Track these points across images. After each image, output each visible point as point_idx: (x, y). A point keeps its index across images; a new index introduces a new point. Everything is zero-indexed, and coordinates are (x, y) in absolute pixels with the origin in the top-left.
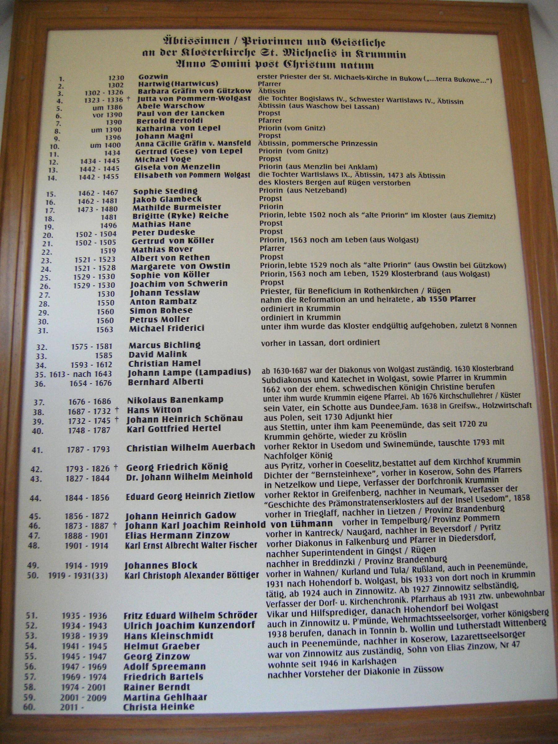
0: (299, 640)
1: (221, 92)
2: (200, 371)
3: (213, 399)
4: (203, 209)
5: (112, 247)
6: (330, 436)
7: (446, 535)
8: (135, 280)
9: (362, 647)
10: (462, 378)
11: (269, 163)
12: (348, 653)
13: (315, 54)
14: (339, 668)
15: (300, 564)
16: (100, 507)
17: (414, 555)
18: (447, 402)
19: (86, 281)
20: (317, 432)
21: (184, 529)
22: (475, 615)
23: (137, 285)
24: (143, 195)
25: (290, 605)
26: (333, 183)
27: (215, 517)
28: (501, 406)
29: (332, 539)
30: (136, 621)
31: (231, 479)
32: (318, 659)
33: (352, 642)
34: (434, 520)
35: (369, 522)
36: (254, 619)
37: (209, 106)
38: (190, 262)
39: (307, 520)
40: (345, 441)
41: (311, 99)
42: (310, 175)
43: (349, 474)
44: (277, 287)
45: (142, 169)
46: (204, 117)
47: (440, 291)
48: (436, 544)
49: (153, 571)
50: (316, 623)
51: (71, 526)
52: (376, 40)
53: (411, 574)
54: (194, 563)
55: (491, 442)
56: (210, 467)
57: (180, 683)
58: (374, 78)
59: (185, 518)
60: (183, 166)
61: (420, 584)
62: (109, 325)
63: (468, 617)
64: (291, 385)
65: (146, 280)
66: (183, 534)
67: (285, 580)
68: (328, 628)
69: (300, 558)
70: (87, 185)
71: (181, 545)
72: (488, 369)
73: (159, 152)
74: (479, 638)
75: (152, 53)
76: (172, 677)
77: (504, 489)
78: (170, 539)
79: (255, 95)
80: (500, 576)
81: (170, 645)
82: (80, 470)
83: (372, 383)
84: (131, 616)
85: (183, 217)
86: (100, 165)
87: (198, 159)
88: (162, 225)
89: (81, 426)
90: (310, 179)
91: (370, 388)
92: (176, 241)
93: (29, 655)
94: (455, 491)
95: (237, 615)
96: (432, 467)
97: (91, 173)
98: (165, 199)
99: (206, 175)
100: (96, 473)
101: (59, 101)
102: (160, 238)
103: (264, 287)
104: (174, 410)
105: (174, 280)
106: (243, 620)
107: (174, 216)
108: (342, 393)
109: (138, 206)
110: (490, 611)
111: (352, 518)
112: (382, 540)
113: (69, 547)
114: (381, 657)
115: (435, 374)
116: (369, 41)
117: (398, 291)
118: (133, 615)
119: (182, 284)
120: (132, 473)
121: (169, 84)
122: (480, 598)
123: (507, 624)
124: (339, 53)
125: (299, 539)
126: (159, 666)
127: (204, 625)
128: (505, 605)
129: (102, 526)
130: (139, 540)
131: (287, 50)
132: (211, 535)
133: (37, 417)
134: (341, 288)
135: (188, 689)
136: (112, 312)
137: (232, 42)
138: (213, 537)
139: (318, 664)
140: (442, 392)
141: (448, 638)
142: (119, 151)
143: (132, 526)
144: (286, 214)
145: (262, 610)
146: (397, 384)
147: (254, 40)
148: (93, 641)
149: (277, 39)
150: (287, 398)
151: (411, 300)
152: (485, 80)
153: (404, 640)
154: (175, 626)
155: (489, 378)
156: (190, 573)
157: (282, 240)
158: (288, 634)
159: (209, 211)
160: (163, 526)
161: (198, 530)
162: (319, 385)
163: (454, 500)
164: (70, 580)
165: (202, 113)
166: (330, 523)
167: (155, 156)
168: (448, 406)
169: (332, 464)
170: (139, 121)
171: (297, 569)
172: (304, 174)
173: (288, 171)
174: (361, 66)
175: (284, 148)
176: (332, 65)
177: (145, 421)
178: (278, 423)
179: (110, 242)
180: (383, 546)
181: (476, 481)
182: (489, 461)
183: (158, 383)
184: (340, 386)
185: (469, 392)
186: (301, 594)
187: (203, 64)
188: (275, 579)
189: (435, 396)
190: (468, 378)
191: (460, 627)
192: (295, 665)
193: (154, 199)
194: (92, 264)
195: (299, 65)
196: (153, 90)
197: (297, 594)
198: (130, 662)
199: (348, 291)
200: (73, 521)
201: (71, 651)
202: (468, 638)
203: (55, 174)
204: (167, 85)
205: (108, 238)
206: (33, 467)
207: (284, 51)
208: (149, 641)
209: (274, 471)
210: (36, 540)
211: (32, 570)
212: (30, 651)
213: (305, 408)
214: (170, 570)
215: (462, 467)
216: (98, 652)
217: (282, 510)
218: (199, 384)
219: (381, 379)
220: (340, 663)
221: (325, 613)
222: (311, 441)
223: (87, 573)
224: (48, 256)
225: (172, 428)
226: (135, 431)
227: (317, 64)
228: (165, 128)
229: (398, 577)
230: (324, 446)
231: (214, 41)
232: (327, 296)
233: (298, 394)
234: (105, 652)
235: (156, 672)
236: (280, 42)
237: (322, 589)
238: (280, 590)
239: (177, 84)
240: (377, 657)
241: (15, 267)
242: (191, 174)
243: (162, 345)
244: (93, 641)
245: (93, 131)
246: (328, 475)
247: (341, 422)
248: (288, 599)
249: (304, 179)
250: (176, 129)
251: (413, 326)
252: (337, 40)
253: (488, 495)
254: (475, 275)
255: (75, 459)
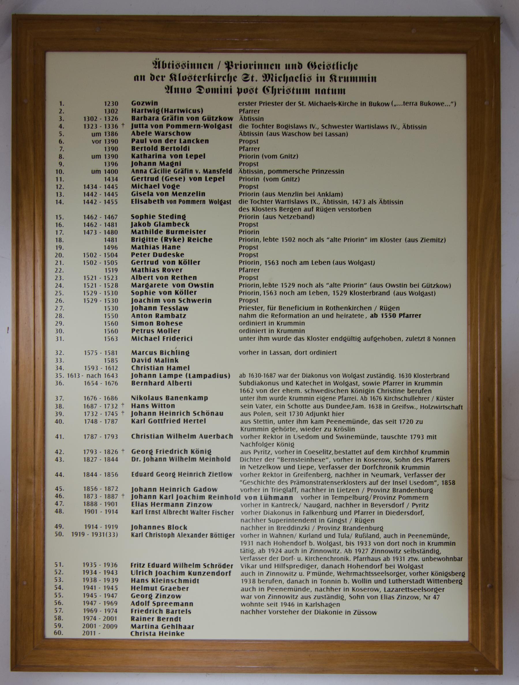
0: (265, 586)
1: (206, 119)
2: (190, 374)
3: (200, 398)
4: (191, 233)
5: (114, 267)
6: (293, 429)
7: (383, 510)
8: (135, 297)
9: (313, 594)
10: (405, 384)
11: (248, 191)
12: (303, 598)
13: (291, 79)
14: (295, 608)
15: (267, 528)
16: (111, 481)
17: (357, 525)
18: (390, 403)
19: (94, 297)
20: (282, 426)
21: (177, 500)
22: (404, 573)
23: (136, 301)
24: (139, 220)
25: (259, 560)
26: (303, 210)
27: (201, 491)
28: (436, 407)
29: (293, 510)
30: (140, 569)
31: (214, 462)
32: (279, 601)
33: (305, 589)
34: (374, 498)
35: (322, 498)
36: (230, 569)
37: (196, 134)
38: (181, 282)
39: (273, 494)
40: (305, 433)
41: (287, 127)
42: (283, 202)
43: (307, 460)
44: (253, 305)
45: (137, 195)
46: (191, 145)
47: (390, 309)
48: (375, 517)
49: (153, 531)
50: (278, 574)
51: (88, 496)
52: (349, 63)
53: (353, 539)
54: (184, 526)
55: (425, 437)
56: (197, 452)
57: (174, 616)
58: (345, 104)
59: (178, 491)
60: (173, 193)
61: (361, 547)
62: (114, 335)
63: (398, 574)
64: (263, 387)
65: (144, 297)
66: (176, 504)
67: (255, 540)
68: (288, 578)
69: (267, 524)
70: (90, 209)
71: (175, 512)
72: (427, 376)
73: (152, 179)
74: (406, 591)
75: (143, 78)
76: (168, 611)
77: (434, 475)
78: (166, 507)
79: (236, 123)
80: (426, 544)
81: (166, 588)
82: (94, 452)
83: (328, 387)
84: (136, 566)
85: (174, 241)
86: (101, 190)
87: (186, 186)
88: (156, 248)
89: (94, 418)
90: (284, 206)
91: (327, 391)
92: (168, 263)
93: (57, 594)
94: (392, 476)
95: (217, 566)
96: (375, 456)
97: (93, 198)
98: (158, 224)
99: (193, 202)
100: (107, 456)
101: (61, 126)
102: (155, 259)
103: (243, 304)
104: (168, 406)
105: (167, 297)
106: (222, 570)
107: (166, 239)
108: (304, 395)
109: (136, 231)
110: (416, 571)
111: (308, 494)
112: (332, 512)
113: (87, 513)
114: (328, 601)
115: (381, 380)
116: (343, 64)
117: (354, 308)
118: (138, 565)
119: (174, 301)
120: (136, 456)
121: (159, 111)
122: (409, 560)
123: (430, 581)
124: (314, 78)
125: (267, 509)
126: (158, 603)
127: (192, 573)
128: (429, 567)
129: (113, 496)
130: (142, 508)
131: (266, 75)
132: (198, 505)
133: (58, 410)
134: (306, 305)
135: (180, 620)
136: (116, 324)
137: (215, 66)
138: (199, 506)
139: (279, 605)
140: (387, 395)
141: (382, 589)
142: (117, 178)
143: (136, 497)
144: (261, 239)
145: (237, 563)
146: (350, 388)
147: (236, 65)
148: (107, 584)
149: (257, 63)
150: (259, 398)
151: (365, 317)
152: (450, 104)
153: (346, 590)
154: (170, 573)
155: (427, 383)
156: (182, 533)
157: (257, 263)
158: (257, 581)
159: (195, 236)
160: (161, 497)
161: (188, 500)
162: (285, 387)
163: (391, 483)
164: (88, 537)
165: (189, 141)
166: (291, 498)
167: (149, 183)
168: (391, 407)
169: (294, 451)
170: (133, 148)
171: (264, 532)
172: (278, 202)
173: (264, 198)
174: (334, 92)
175: (261, 176)
176: (307, 91)
177: (145, 414)
178: (251, 418)
179: (112, 263)
180: (332, 517)
181: (411, 468)
182: (422, 452)
183: (155, 384)
184: (302, 388)
185: (409, 395)
186: (267, 551)
187: (189, 91)
188: (247, 539)
189: (380, 398)
190: (409, 384)
191: (391, 582)
192: (261, 605)
193: (149, 224)
194: (98, 282)
195: (277, 91)
196: (144, 116)
197: (264, 551)
198: (136, 600)
199: (312, 308)
200: (90, 492)
201: (90, 592)
202: (397, 590)
203: (61, 198)
204: (158, 112)
205: (111, 259)
206: (57, 450)
207: (263, 76)
208: (150, 584)
209: (247, 456)
210: (61, 507)
211: (58, 530)
212: (58, 591)
213: (273, 406)
214: (166, 531)
215: (400, 456)
216: (111, 592)
217: (253, 487)
218: (188, 385)
219: (336, 383)
220: (296, 605)
221: (285, 566)
222: (278, 433)
223: (102, 532)
224: (60, 274)
225: (167, 420)
226: (138, 422)
227: (293, 89)
228: (156, 156)
229: (343, 541)
230: (288, 437)
231: (199, 66)
232: (294, 312)
233: (268, 395)
234: (116, 592)
235: (155, 608)
236: (260, 66)
237: (284, 548)
238: (250, 547)
239: (166, 111)
240: (325, 601)
241: (33, 283)
242: (180, 201)
243: (158, 353)
244: (107, 584)
245: (93, 157)
246: (290, 460)
247: (302, 418)
248: (257, 555)
249: (278, 206)
250: (166, 157)
251: (365, 339)
252: (313, 64)
253: (420, 479)
254: (422, 294)
255: (90, 444)
